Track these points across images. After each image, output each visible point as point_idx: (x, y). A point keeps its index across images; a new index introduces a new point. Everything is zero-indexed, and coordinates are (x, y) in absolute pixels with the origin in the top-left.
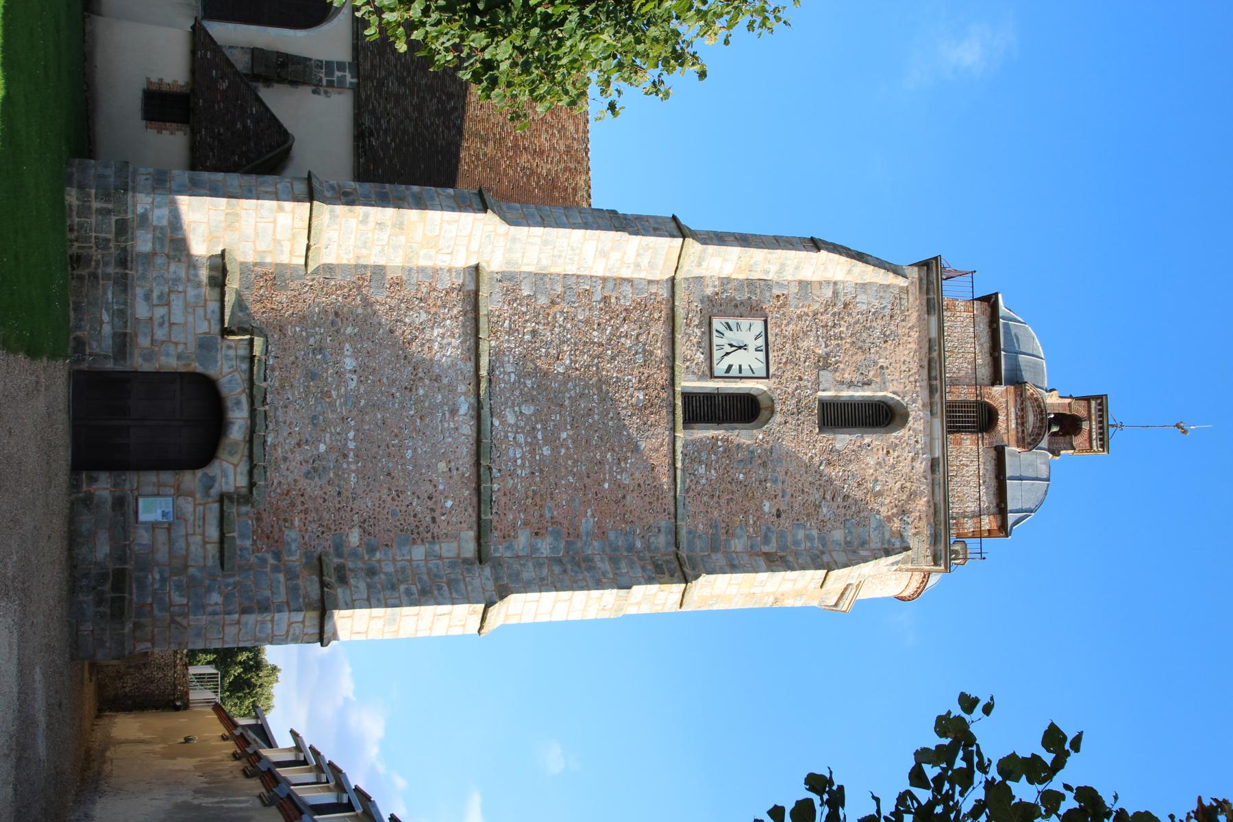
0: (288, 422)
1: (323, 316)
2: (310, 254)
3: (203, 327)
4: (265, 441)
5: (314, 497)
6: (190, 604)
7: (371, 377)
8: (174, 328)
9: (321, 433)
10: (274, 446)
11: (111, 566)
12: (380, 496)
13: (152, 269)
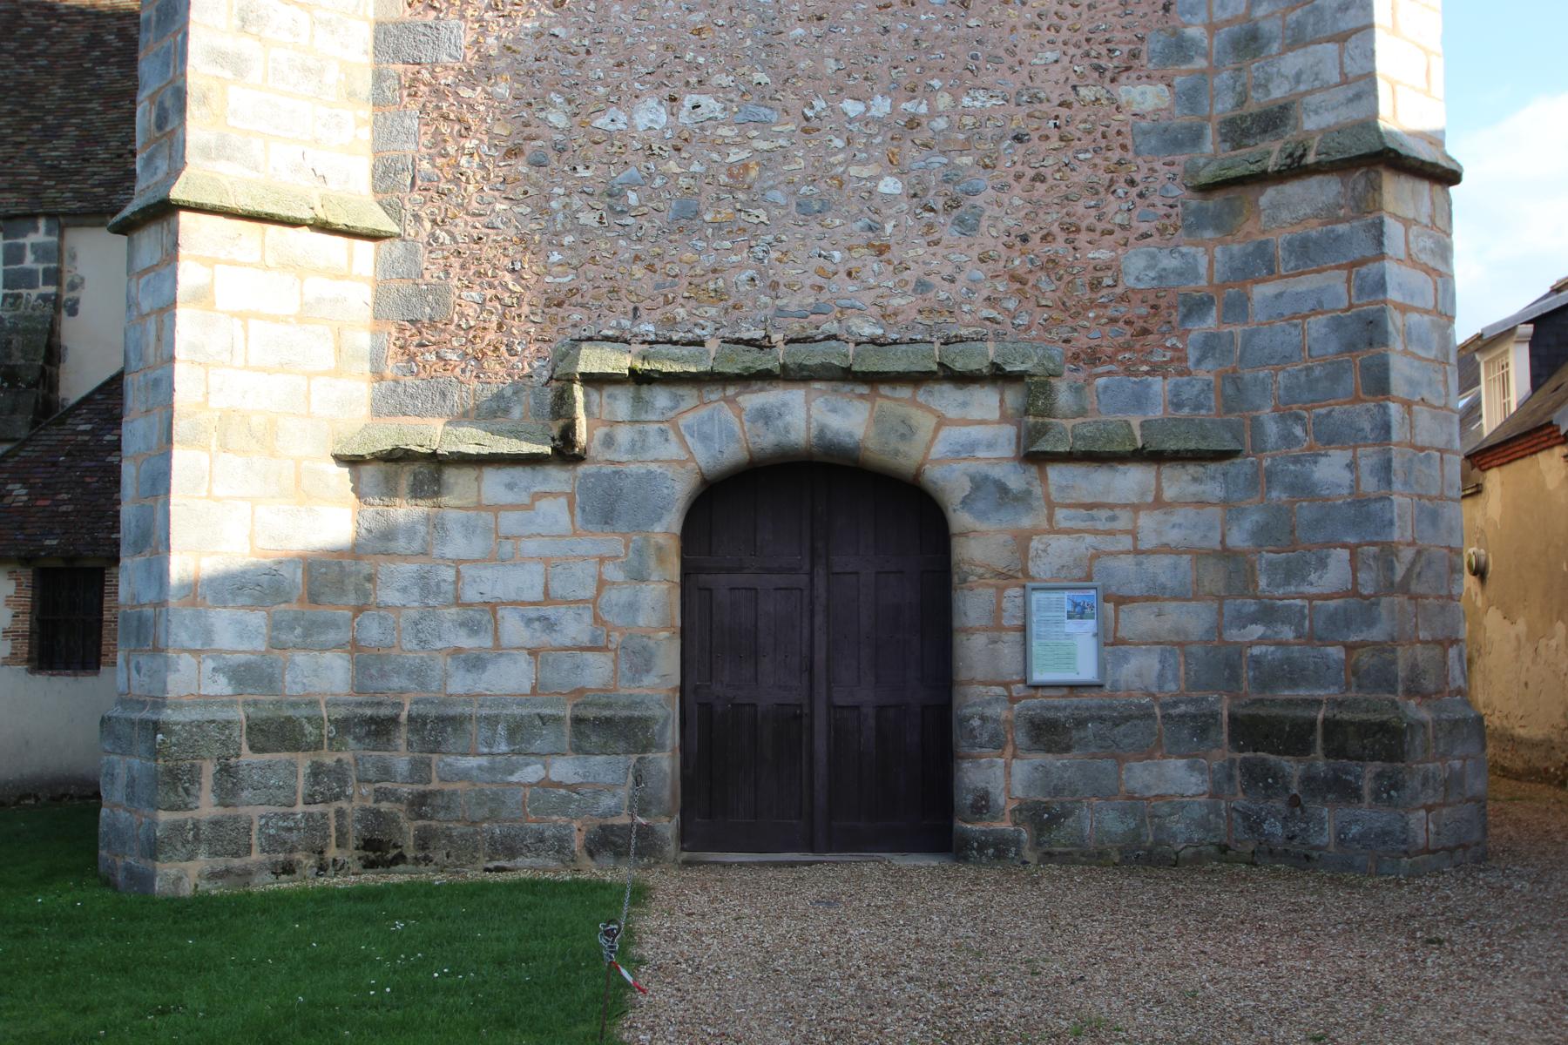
0: (819, 281)
1: (520, 190)
2: (339, 220)
3: (555, 514)
4: (873, 341)
5: (1029, 207)
6: (1351, 540)
7: (689, 56)
8: (557, 589)
9: (847, 190)
10: (886, 316)
11: (1221, 754)
12: (1029, 26)
13: (394, 652)
